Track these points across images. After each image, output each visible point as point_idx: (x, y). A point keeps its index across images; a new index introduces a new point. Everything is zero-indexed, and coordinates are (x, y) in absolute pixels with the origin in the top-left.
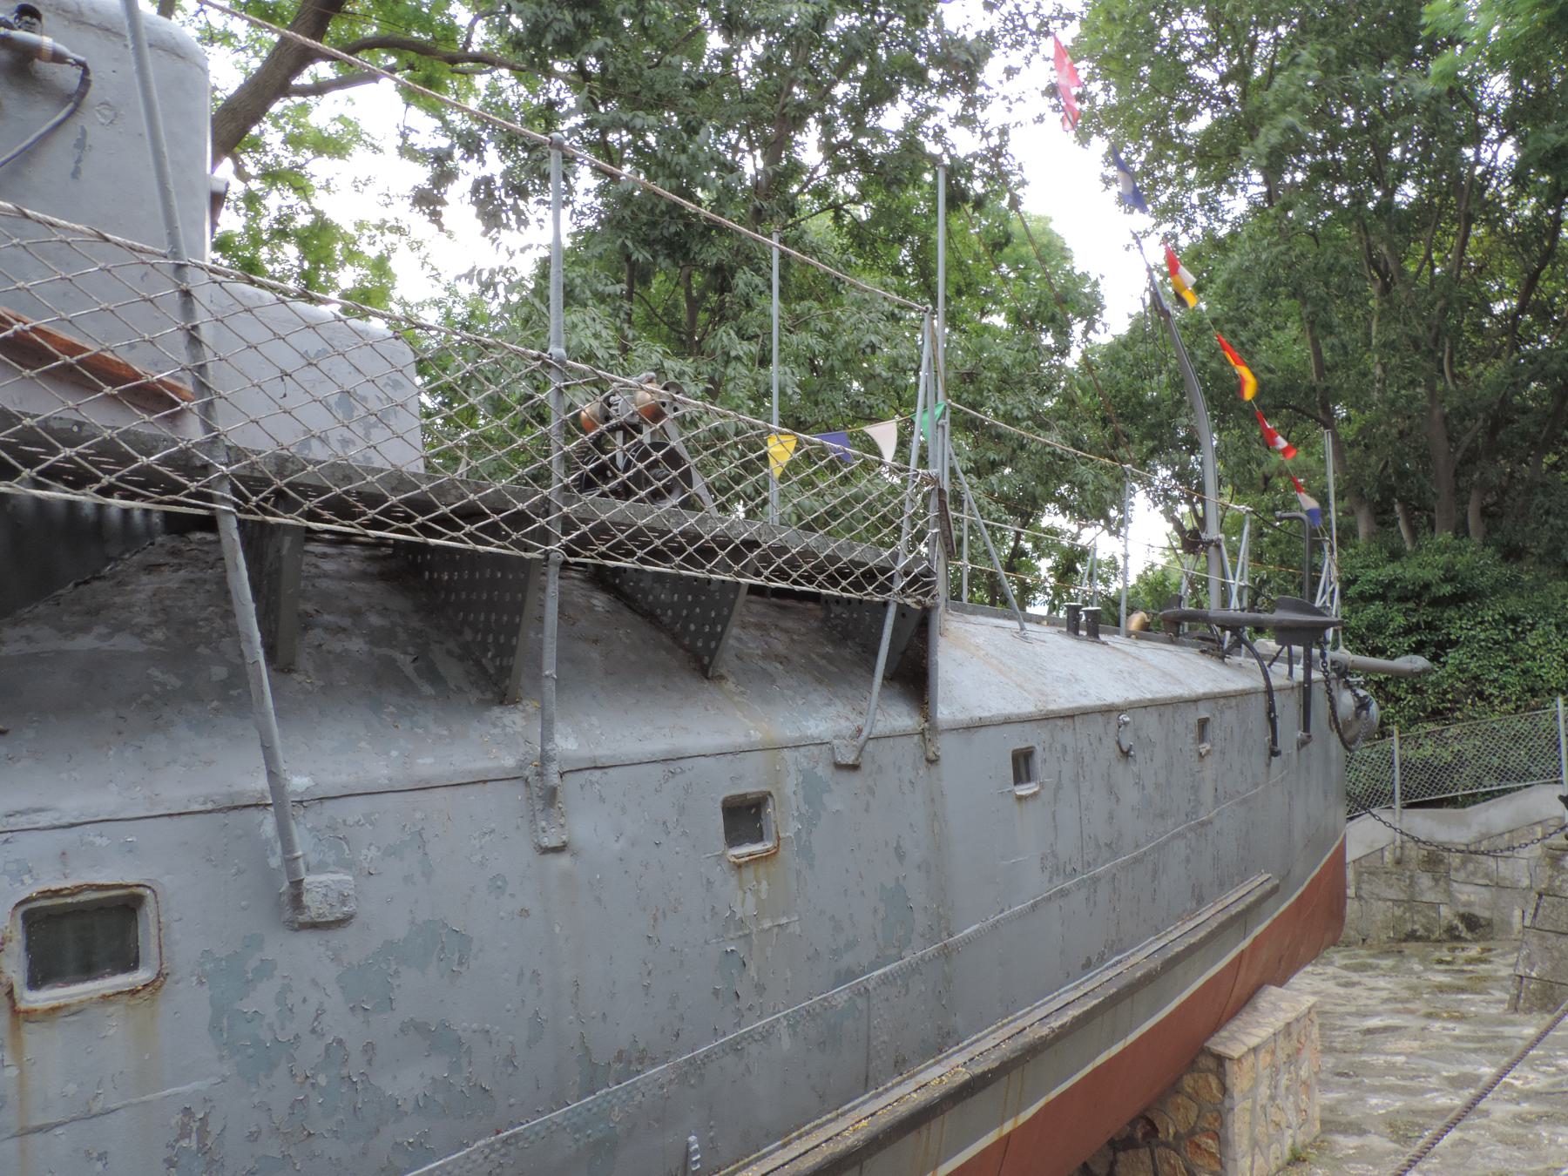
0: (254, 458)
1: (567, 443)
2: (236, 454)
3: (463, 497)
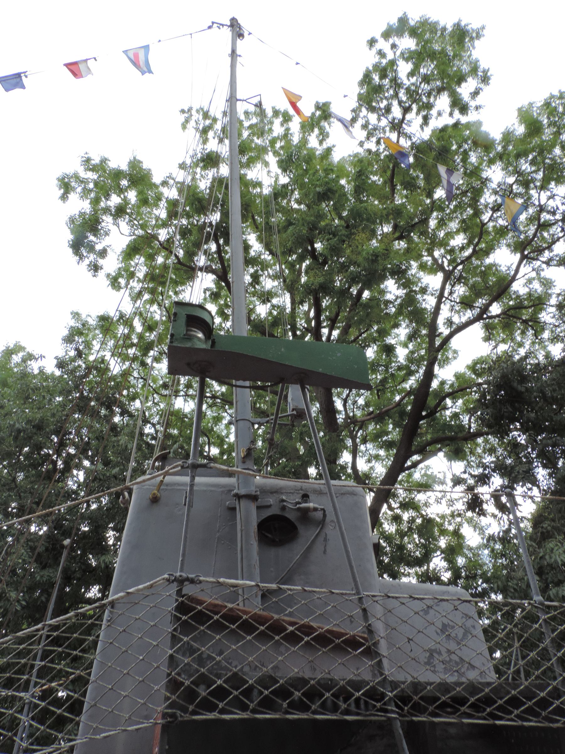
0: (402, 686)
1: (559, 651)
2: (394, 685)
3: (509, 693)
